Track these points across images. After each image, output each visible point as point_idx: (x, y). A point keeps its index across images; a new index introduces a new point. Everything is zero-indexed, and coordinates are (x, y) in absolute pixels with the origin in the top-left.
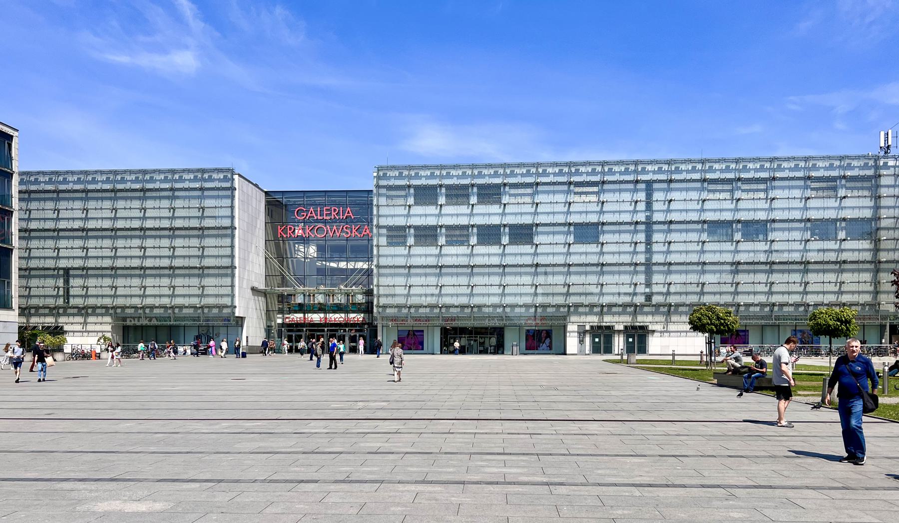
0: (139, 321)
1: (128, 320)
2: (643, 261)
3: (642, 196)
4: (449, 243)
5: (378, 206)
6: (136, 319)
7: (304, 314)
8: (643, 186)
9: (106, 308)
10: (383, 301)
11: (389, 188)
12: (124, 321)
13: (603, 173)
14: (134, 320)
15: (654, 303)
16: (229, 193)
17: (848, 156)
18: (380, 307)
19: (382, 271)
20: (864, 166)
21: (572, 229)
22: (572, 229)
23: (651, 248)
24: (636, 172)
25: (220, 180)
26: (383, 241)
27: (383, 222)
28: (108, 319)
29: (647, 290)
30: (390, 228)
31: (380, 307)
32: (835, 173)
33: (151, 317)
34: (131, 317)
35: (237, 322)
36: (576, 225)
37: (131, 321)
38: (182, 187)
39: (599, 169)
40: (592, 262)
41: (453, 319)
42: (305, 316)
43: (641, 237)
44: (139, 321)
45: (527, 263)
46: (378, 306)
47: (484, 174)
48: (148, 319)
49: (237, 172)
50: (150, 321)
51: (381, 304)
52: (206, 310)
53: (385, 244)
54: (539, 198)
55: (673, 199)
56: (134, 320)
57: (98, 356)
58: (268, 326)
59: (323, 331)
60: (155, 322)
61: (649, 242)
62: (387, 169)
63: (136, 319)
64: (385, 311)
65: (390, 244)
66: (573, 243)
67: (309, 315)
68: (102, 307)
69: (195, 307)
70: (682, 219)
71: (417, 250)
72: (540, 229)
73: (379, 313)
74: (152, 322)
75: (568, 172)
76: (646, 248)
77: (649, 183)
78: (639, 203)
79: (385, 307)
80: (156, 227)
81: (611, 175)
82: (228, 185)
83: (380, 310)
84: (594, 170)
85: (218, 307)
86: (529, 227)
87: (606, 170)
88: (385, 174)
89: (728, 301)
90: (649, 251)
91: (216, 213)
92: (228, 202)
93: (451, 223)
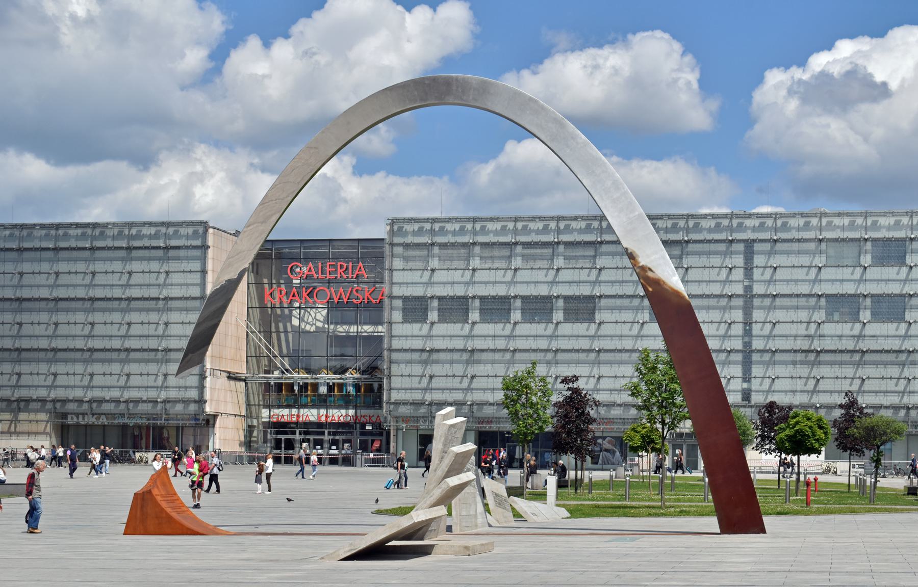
0: (84, 419)
1: (69, 417)
2: (740, 347)
3: (739, 260)
4: (442, 320)
5: (391, 270)
6: (81, 417)
7: (298, 409)
8: (741, 247)
9: (43, 401)
10: (395, 396)
11: (407, 246)
12: (62, 419)
13: (515, 232)
14: (78, 418)
15: (753, 403)
16: (198, 253)
17: (693, 215)
18: (391, 404)
19: (395, 356)
20: (895, 224)
21: (823, 301)
22: (823, 301)
23: (751, 329)
24: (432, 232)
25: (187, 237)
26: (397, 316)
27: (397, 291)
28: (43, 416)
29: (745, 385)
30: (405, 299)
31: (391, 404)
32: (467, 239)
33: (99, 414)
34: (74, 414)
35: (208, 421)
36: (828, 296)
37: (72, 418)
38: (32, 246)
39: (511, 226)
40: (457, 347)
41: (489, 421)
42: (299, 411)
43: (738, 315)
44: (84, 419)
45: (458, 348)
46: (389, 403)
47: (572, 229)
48: (95, 416)
49: (211, 224)
50: (98, 419)
51: (393, 400)
52: (131, 405)
53: (401, 320)
54: (601, 262)
55: (689, 266)
56: (78, 418)
57: (913, 460)
58: (249, 427)
59: (323, 433)
60: (104, 420)
61: (748, 323)
62: (403, 222)
63: (81, 417)
64: (397, 409)
65: (405, 320)
66: (869, 322)
67: (306, 410)
68: (38, 400)
69: (155, 402)
70: (180, 295)
71: (440, 329)
72: (603, 302)
73: (390, 412)
74: (101, 420)
75: (598, 228)
76: (745, 330)
77: (749, 244)
78: (733, 269)
79: (397, 404)
80: (108, 297)
81: (762, 232)
82: (198, 243)
83: (392, 407)
84: (807, 224)
85: (184, 402)
86: (591, 298)
87: (735, 225)
88: (400, 229)
89: (803, 401)
90: (748, 333)
91: (37, 280)
92: (197, 266)
93: (570, 293)
